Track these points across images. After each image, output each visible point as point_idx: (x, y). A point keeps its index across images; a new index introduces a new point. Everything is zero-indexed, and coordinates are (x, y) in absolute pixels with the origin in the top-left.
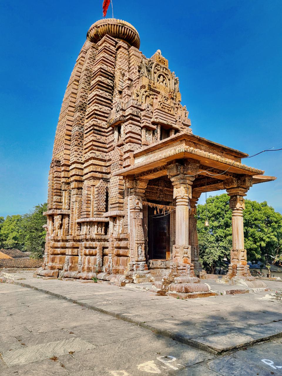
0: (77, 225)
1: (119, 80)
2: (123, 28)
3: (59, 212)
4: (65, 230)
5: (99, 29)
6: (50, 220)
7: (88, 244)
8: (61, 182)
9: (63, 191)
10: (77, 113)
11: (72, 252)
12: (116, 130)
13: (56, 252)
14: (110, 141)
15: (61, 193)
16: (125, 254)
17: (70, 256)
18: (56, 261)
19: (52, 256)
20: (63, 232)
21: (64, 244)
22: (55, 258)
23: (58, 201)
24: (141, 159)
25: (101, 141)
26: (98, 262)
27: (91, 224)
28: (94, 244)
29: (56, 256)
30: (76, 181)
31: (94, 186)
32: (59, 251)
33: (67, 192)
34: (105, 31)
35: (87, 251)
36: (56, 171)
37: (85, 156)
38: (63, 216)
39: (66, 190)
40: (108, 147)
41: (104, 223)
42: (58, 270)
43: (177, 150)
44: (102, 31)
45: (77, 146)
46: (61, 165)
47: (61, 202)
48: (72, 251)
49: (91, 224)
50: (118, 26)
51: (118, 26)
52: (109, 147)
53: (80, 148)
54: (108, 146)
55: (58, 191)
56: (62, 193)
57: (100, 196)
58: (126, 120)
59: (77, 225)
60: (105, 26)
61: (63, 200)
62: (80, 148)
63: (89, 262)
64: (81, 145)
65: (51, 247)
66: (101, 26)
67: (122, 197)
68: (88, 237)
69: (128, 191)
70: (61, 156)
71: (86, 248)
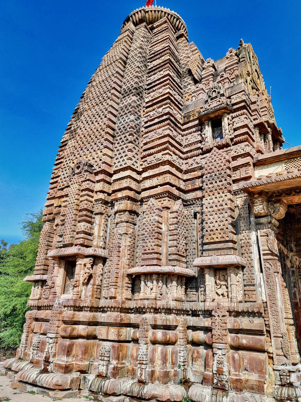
0: (127, 280)
1: (198, 66)
2: (178, 21)
3: (90, 251)
4: (95, 287)
5: (147, 14)
6: (60, 267)
7: (161, 319)
8: (93, 200)
9: (96, 214)
10: (132, 97)
11: (119, 335)
12: (208, 125)
13: (75, 333)
14: (190, 142)
15: (91, 217)
16: (258, 346)
17: (111, 343)
18: (74, 352)
19: (68, 342)
20: (93, 291)
21: (94, 317)
22: (73, 345)
23: (87, 231)
24: (273, 168)
25: (177, 139)
26: (182, 360)
27: (166, 277)
28: (171, 319)
29: (74, 341)
30: (129, 198)
31: (168, 208)
32: (81, 329)
33: (103, 217)
34: (155, 18)
35: (159, 334)
36: (89, 180)
37: (51, 193)
38: (97, 259)
39: (102, 214)
40: (185, 151)
41: (185, 279)
42: (79, 373)
43: (240, 186)
44: (151, 17)
45: (132, 143)
46: (95, 171)
47: (90, 234)
48: (119, 332)
49: (166, 277)
50: (173, 17)
51: (173, 17)
52: (187, 152)
53: (136, 147)
54: (185, 150)
55: (89, 214)
56: (94, 218)
57: (180, 227)
58: (234, 109)
59: (127, 278)
60: (157, 12)
61: (96, 231)
62: (136, 147)
63: (164, 360)
64: (137, 143)
65: (65, 322)
66: (151, 11)
67: (235, 232)
68: (160, 304)
69: (250, 222)
70: (97, 157)
71: (155, 327)
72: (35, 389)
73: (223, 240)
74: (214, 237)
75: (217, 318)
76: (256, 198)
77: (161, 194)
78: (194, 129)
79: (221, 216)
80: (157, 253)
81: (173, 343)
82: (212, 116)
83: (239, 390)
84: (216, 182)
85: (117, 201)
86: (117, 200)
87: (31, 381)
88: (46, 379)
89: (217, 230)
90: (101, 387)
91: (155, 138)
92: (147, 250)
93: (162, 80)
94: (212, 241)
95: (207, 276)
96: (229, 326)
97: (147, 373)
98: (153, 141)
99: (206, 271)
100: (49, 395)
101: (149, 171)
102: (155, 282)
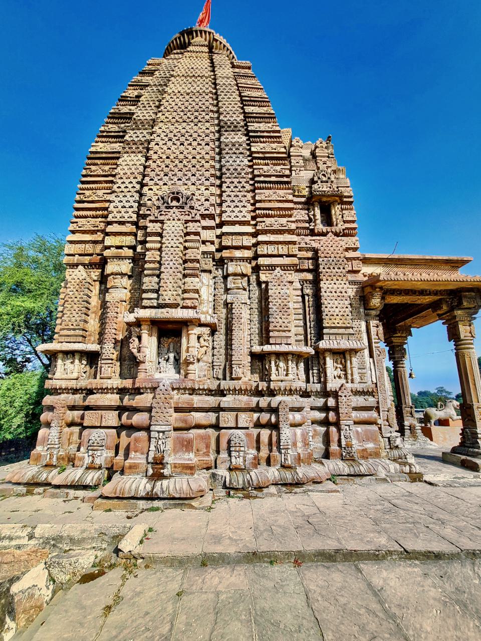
72: (156, 504)
73: (344, 325)
74: (336, 322)
75: (344, 398)
76: (377, 292)
77: (287, 265)
78: (300, 206)
79: (342, 302)
80: (84, 330)
81: (300, 425)
82: (324, 199)
83: (365, 458)
84: (334, 268)
85: (232, 261)
86: (231, 259)
87: (143, 494)
88: (131, 486)
89: (337, 315)
90: (249, 481)
91: (275, 199)
92: (278, 327)
93: (272, 134)
94: (333, 325)
95: (328, 359)
96: (354, 405)
97: (293, 457)
98: (270, 201)
99: (327, 354)
100: (192, 507)
101: (268, 235)
102: (77, 361)
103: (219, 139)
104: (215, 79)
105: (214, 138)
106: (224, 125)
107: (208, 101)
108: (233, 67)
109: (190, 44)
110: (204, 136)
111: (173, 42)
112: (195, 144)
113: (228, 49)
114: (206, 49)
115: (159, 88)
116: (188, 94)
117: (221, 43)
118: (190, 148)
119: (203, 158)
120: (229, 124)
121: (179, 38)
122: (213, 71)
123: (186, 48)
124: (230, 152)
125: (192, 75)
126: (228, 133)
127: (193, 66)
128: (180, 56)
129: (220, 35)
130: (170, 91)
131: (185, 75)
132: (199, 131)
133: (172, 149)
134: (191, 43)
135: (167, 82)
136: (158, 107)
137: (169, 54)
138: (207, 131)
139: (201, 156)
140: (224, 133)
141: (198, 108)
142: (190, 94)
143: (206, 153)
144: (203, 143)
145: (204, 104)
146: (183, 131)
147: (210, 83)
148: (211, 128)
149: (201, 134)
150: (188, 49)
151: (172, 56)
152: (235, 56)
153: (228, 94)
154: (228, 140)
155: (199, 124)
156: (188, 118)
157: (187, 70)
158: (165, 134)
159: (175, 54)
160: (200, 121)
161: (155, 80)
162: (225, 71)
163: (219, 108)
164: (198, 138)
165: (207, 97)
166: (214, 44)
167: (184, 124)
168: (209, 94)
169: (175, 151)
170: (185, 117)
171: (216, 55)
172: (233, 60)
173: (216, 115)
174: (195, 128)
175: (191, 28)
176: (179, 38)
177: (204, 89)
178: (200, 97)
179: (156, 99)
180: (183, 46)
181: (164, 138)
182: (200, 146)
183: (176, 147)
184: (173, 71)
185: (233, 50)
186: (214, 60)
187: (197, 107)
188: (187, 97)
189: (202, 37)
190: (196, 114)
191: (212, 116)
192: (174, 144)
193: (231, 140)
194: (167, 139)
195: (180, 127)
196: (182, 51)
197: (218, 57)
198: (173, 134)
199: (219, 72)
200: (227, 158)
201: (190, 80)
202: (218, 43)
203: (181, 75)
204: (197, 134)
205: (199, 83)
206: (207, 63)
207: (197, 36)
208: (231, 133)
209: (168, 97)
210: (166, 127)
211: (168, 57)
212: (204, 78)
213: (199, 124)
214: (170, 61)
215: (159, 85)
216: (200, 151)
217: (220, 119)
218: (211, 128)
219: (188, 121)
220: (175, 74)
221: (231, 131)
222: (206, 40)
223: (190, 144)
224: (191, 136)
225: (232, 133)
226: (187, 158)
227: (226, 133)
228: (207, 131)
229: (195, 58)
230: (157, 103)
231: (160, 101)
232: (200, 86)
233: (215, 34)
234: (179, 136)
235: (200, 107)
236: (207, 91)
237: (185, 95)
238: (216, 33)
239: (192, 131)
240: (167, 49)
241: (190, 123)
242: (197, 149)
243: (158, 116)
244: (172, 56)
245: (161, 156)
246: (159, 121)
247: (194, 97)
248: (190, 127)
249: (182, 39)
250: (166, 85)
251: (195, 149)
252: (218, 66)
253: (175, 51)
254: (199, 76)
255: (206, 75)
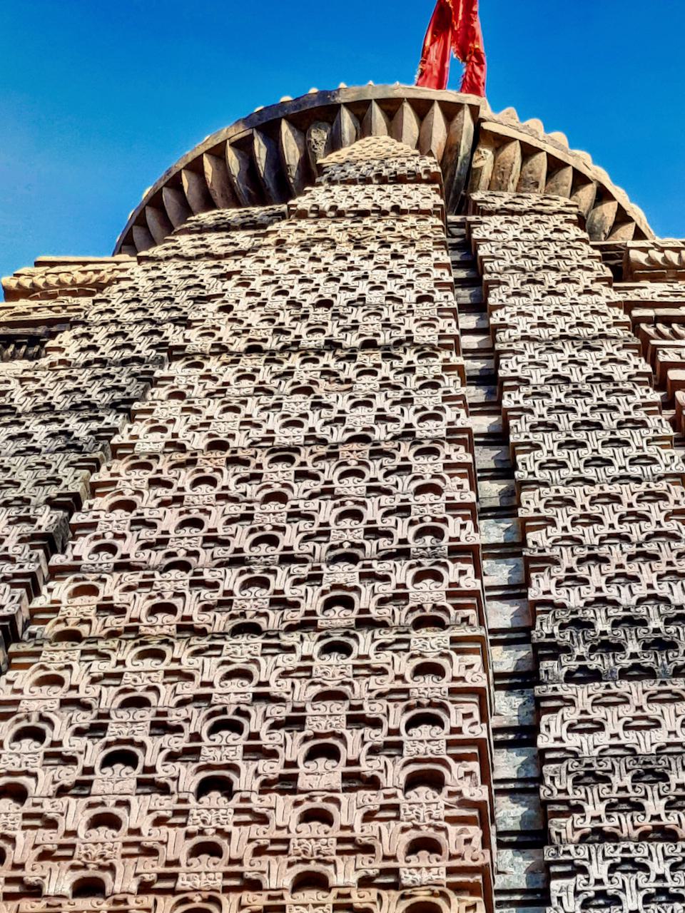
103: (523, 736)
104: (491, 353)
105: (481, 732)
106: (564, 638)
107: (443, 488)
108: (622, 269)
109: (310, 173)
110: (398, 719)
111: (195, 167)
112: (321, 777)
113: (580, 180)
114: (426, 196)
115: (72, 423)
116: (284, 455)
117: (528, 151)
118: (284, 810)
119: (408, 434)
120: (602, 625)
121: (244, 146)
122: (480, 307)
123: (286, 193)
124: (625, 823)
125: (320, 339)
126: (597, 688)
127: (328, 290)
128: (243, 239)
129: (523, 117)
130: (149, 443)
131: (272, 344)
132: (360, 690)
133: (130, 821)
134: (321, 169)
135: (134, 389)
136: (50, 543)
137: (169, 228)
138: (426, 688)
139: (370, 865)
140: (567, 690)
141: (359, 537)
142: (304, 455)
143: (415, 847)
144: (394, 774)
145: (404, 510)
146: (233, 694)
147: (451, 383)
148: (456, 666)
149: (373, 709)
150: (302, 202)
151: (184, 240)
152: (636, 212)
153: (594, 440)
154: (603, 739)
155: (364, 644)
156: (279, 602)
157: (285, 318)
158: (84, 719)
159: (203, 229)
160: (366, 623)
161: (47, 379)
162: (555, 305)
163: (524, 526)
164: (353, 736)
165: (427, 467)
166: (485, 160)
167: (243, 649)
168: (447, 449)
169: (151, 835)
170: (253, 602)
171: (496, 221)
172: (625, 235)
173: (499, 573)
174: (332, 669)
175: (323, 95)
176: (244, 146)
177: (410, 417)
178: (374, 470)
179: (41, 495)
180: (271, 188)
181: (72, 745)
182: (364, 795)
183: (165, 805)
184: (185, 323)
185: (615, 181)
186: (483, 251)
187: (349, 532)
188: (278, 474)
189: (395, 131)
190: (345, 574)
191: (469, 583)
192: (149, 785)
193: (629, 738)
194: (94, 753)
195: (211, 669)
196: (256, 210)
197: (512, 232)
198: (147, 715)
199: (515, 312)
200: (598, 870)
201: (305, 372)
202: (513, 152)
203: (240, 344)
204: (341, 709)
205: (367, 385)
206: (430, 266)
207: (364, 129)
208: (624, 686)
209: (131, 482)
210: (99, 667)
211: (158, 251)
212: (411, 356)
213: (364, 644)
214: (169, 269)
215: (75, 408)
216: (364, 832)
217: (534, 594)
218: (456, 666)
219: (274, 620)
220: (196, 341)
221: (624, 674)
222: (422, 146)
223: (286, 783)
224: (295, 722)
225: (636, 690)
226: (255, 886)
227: (583, 694)
228: (426, 688)
229: (344, 248)
230: (46, 519)
231: (72, 503)
232: (379, 402)
233: (485, 112)
234: (199, 723)
235: (373, 532)
236: (435, 429)
237: (264, 459)
238: (497, 108)
239: (303, 692)
240: (155, 201)
241: (288, 640)
242: (341, 818)
243: (41, 602)
244: (186, 243)
245: (30, 876)
246: (50, 629)
247: (330, 471)
248: (292, 661)
249: (260, 150)
250: (123, 407)
251: (325, 818)
252: (514, 281)
253: (207, 217)
254: (369, 345)
255: (426, 336)
